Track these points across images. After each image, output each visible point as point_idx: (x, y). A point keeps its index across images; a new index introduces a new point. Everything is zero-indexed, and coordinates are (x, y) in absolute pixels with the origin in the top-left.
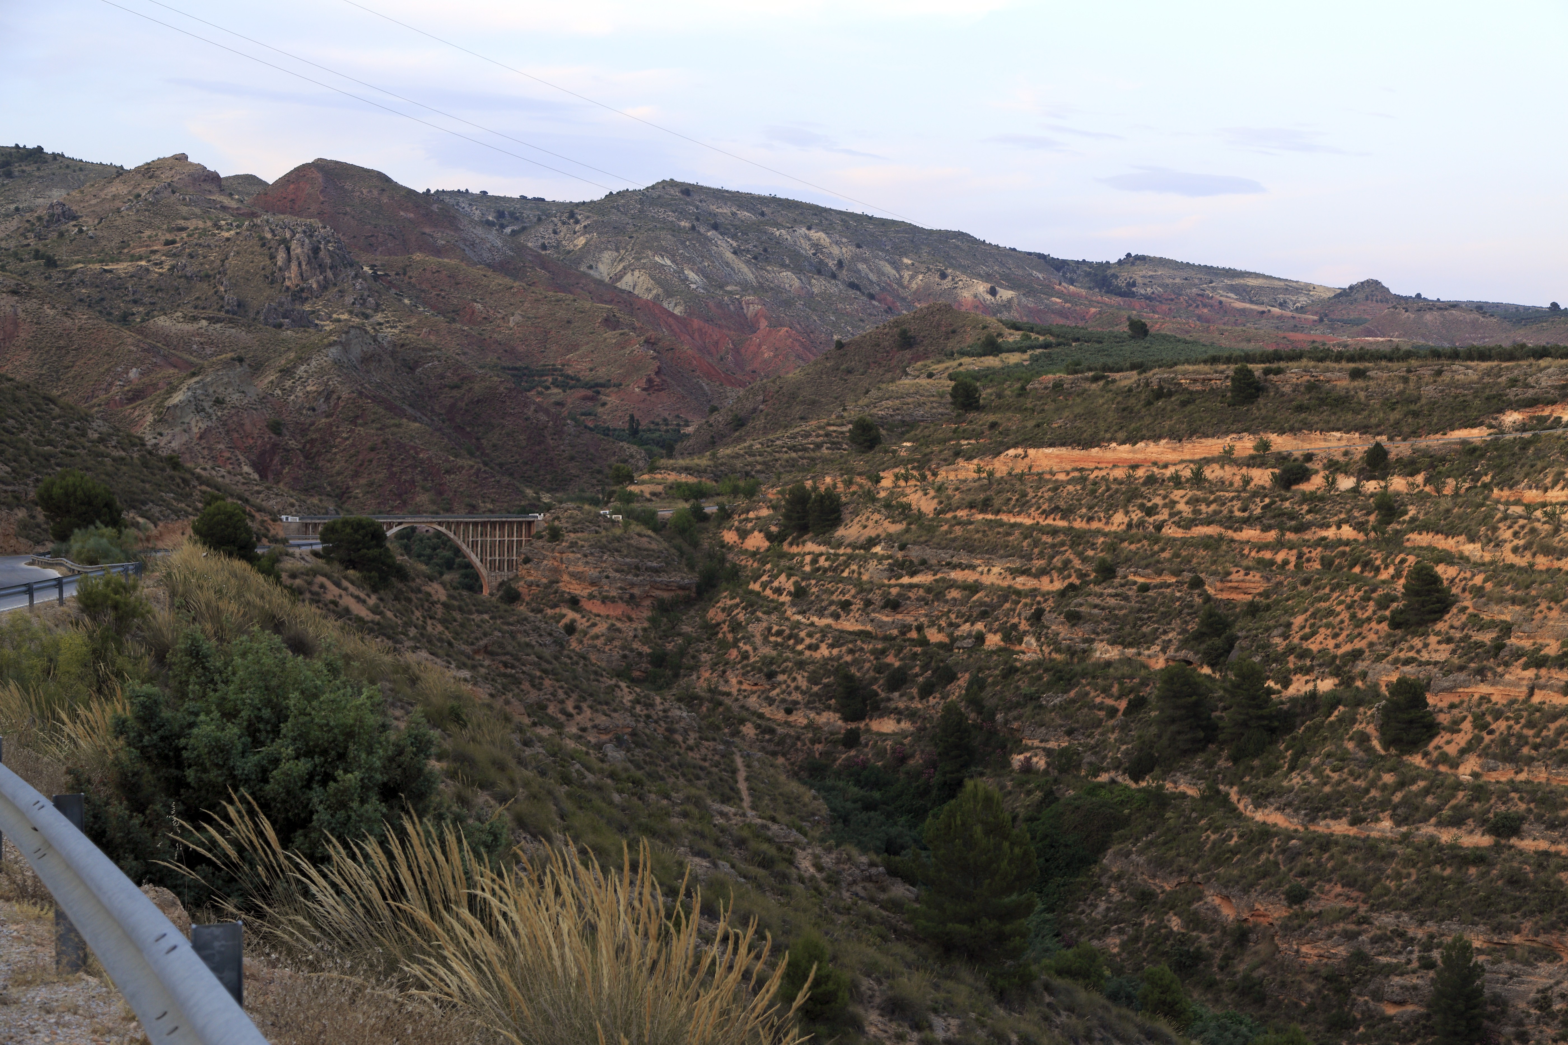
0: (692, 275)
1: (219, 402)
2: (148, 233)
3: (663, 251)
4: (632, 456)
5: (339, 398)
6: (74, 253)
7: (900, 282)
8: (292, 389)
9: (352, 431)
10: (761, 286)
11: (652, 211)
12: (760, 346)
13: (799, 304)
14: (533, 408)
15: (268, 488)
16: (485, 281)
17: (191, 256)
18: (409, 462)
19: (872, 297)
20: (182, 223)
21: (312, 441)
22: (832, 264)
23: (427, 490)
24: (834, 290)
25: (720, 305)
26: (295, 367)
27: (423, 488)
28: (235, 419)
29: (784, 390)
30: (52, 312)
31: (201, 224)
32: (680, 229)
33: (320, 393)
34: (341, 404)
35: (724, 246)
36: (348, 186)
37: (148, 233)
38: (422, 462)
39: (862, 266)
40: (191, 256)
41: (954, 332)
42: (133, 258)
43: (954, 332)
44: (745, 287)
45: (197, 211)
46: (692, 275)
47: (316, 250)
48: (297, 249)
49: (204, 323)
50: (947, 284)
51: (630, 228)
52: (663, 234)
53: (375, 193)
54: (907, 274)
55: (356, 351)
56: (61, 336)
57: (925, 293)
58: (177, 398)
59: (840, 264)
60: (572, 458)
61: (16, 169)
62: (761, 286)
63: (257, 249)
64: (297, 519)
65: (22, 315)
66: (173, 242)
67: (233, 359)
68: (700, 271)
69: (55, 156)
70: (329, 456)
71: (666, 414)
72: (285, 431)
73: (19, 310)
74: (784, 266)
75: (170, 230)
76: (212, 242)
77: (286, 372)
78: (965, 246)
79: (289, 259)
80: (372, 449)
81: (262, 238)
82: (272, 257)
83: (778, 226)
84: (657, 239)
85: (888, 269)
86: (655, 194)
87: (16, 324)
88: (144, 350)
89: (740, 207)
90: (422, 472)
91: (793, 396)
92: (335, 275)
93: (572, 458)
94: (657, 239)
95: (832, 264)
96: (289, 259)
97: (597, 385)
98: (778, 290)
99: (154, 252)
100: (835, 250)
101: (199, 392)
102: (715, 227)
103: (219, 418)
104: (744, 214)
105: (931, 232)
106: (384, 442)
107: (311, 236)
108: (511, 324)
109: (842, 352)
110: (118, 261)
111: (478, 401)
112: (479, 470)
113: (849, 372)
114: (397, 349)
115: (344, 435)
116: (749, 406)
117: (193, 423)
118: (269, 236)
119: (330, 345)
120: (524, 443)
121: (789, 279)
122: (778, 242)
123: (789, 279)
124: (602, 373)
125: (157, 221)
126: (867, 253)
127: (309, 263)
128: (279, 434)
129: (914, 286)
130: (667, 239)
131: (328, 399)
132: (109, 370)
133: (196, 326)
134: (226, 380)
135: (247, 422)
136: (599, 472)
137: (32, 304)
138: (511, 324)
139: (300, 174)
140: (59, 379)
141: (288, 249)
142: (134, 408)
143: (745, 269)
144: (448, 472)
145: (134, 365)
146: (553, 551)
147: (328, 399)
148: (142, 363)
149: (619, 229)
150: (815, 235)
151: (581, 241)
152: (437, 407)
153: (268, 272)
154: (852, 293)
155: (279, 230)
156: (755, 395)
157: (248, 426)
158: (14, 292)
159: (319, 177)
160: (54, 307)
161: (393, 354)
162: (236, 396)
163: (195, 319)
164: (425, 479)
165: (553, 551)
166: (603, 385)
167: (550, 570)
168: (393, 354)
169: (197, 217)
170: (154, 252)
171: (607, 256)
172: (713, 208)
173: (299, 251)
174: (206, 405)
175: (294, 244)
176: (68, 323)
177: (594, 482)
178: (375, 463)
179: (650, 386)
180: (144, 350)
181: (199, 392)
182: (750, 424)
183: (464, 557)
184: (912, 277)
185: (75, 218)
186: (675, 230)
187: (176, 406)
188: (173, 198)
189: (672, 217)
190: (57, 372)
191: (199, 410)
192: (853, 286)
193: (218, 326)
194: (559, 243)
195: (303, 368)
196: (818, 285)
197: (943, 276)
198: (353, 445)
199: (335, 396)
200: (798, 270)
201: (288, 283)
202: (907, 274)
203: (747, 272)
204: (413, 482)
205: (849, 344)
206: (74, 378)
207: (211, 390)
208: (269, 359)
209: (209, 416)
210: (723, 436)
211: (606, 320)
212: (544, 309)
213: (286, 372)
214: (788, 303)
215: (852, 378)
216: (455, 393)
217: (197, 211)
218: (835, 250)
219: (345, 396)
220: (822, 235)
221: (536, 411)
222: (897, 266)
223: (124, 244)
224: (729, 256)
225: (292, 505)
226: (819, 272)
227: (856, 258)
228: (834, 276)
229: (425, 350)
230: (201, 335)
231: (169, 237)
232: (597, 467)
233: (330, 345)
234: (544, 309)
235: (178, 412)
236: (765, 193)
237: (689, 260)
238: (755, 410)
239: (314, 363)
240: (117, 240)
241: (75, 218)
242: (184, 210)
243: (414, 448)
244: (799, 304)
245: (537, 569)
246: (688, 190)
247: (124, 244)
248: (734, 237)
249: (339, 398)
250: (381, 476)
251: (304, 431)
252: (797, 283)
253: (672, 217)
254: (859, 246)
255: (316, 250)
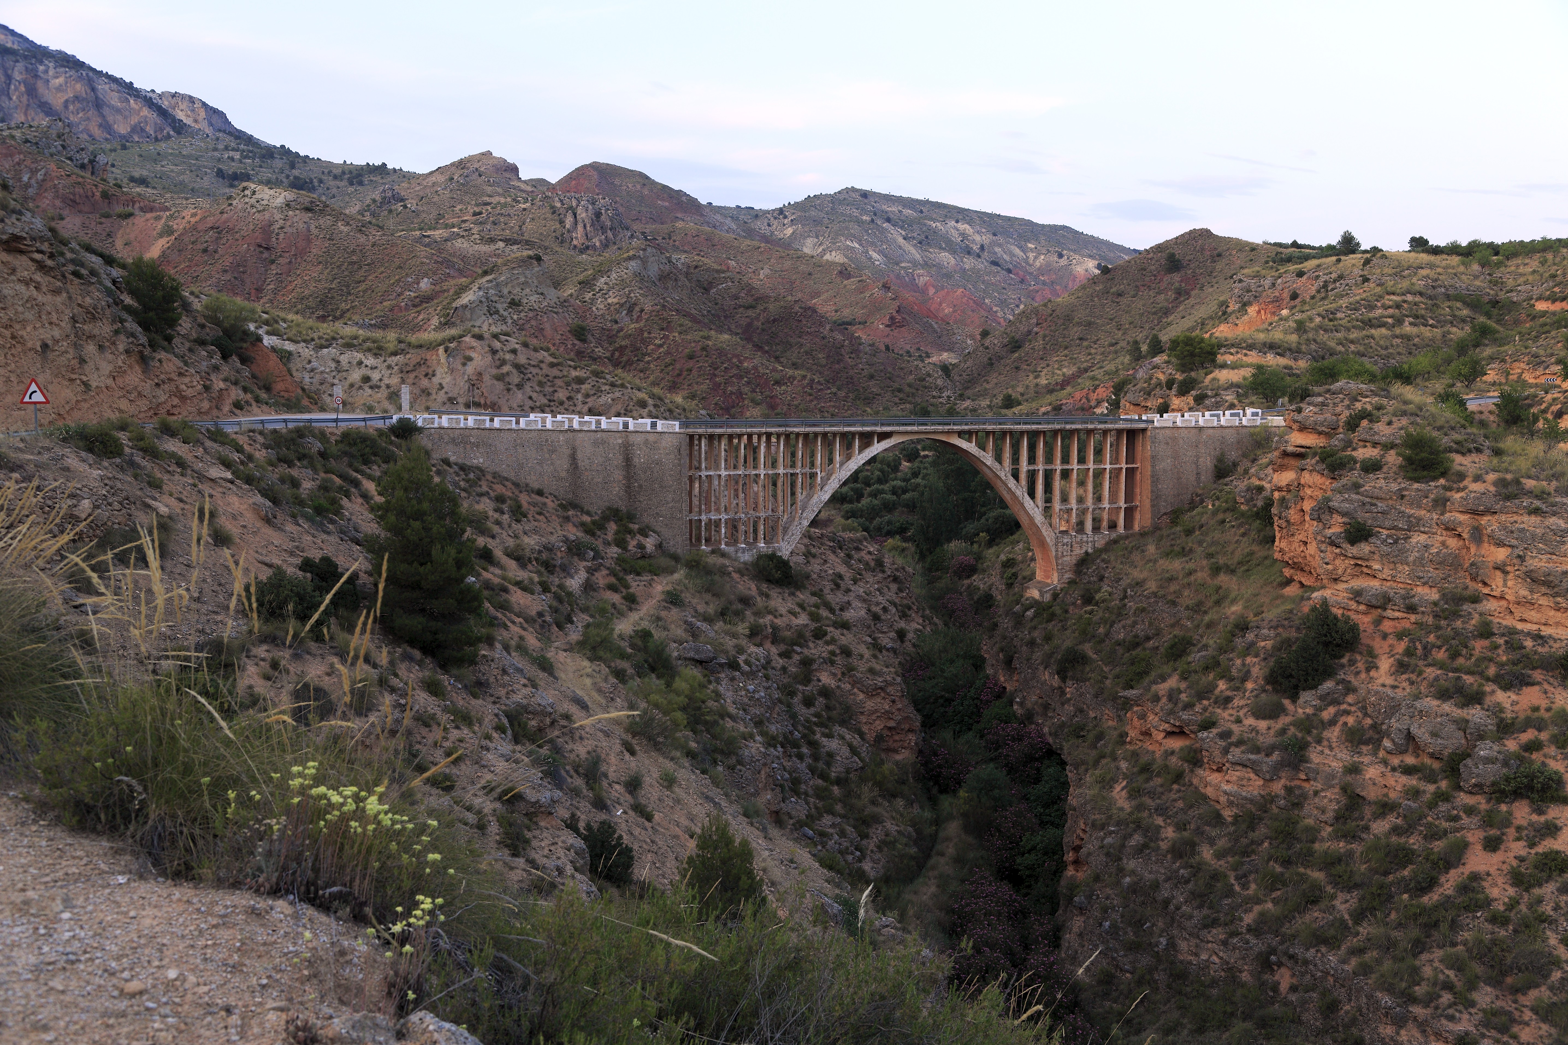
0: (875, 255)
1: (514, 304)
2: (459, 207)
3: (852, 237)
4: (929, 375)
5: (642, 311)
6: (399, 224)
7: (1026, 260)
8: (593, 301)
9: (665, 337)
10: (926, 263)
11: (841, 209)
12: (940, 304)
13: (957, 277)
14: (828, 327)
15: (597, 374)
16: (736, 243)
17: (494, 223)
18: (735, 371)
19: (1009, 271)
20: (487, 199)
21: (622, 349)
22: (976, 248)
23: (757, 404)
24: (981, 266)
25: (898, 276)
26: (594, 279)
27: (753, 401)
28: (533, 323)
29: (1058, 312)
30: (345, 229)
31: (502, 200)
32: (863, 222)
33: (622, 305)
34: (645, 316)
35: (896, 235)
36: (617, 182)
37: (459, 207)
38: (747, 372)
39: (998, 250)
40: (494, 223)
41: (1219, 255)
42: (446, 226)
43: (1219, 255)
44: (915, 264)
45: (500, 190)
46: (875, 255)
47: (598, 215)
48: (582, 214)
49: (501, 244)
50: (1063, 262)
51: (826, 221)
52: (851, 225)
53: (638, 187)
54: (1031, 255)
55: (654, 270)
56: (354, 251)
57: (1046, 269)
58: (467, 298)
59: (982, 248)
60: (872, 377)
61: (366, 180)
62: (926, 263)
63: (549, 215)
64: (675, 425)
65: (315, 231)
66: (480, 213)
67: (530, 257)
68: (880, 252)
69: (394, 170)
70: (641, 365)
71: (908, 347)
72: (590, 337)
73: (312, 227)
74: (941, 248)
75: (477, 205)
76: (512, 212)
77: (586, 284)
78: (1070, 236)
79: (576, 223)
80: (691, 357)
81: (553, 207)
82: (562, 222)
83: (935, 220)
84: (847, 228)
85: (1017, 251)
86: (842, 197)
87: (309, 240)
88: (436, 262)
89: (905, 206)
90: (748, 383)
91: (1068, 318)
92: (615, 236)
93: (872, 377)
94: (847, 228)
95: (976, 248)
96: (576, 223)
97: (844, 323)
98: (939, 266)
99: (464, 221)
100: (977, 238)
101: (492, 292)
102: (888, 220)
103: (514, 322)
104: (908, 212)
105: (1043, 226)
106: (704, 349)
107: (593, 204)
108: (762, 277)
109: (1108, 276)
110: (435, 229)
111: (774, 321)
112: (812, 380)
113: (1120, 295)
114: (690, 271)
115: (658, 342)
116: (1023, 328)
117: (485, 327)
118: (558, 205)
119: (630, 258)
120: (824, 361)
121: (946, 258)
122: (935, 232)
123: (946, 258)
124: (846, 313)
125: (467, 198)
126: (1000, 239)
127: (592, 225)
128: (584, 341)
129: (1038, 264)
130: (855, 229)
131: (630, 311)
132: (399, 280)
133: (493, 247)
134: (522, 279)
135: (547, 326)
136: (900, 390)
137: (326, 221)
138: (762, 277)
139: (580, 173)
140: (349, 294)
141: (575, 215)
142: (419, 312)
143: (913, 251)
144: (777, 383)
145: (426, 275)
146: (1441, 504)
147: (630, 311)
148: (435, 273)
149: (817, 222)
150: (960, 226)
151: (789, 231)
152: (733, 327)
153: (558, 234)
154: (994, 268)
155: (566, 200)
156: (1028, 318)
157: (548, 331)
158: (308, 209)
159: (595, 175)
160: (348, 224)
161: (687, 274)
162: (534, 298)
163: (492, 240)
164: (754, 391)
165: (1441, 504)
166: (850, 324)
167: (1440, 562)
168: (687, 274)
169: (499, 195)
170: (464, 221)
171: (810, 242)
172: (884, 207)
173: (584, 215)
174: (500, 307)
175: (579, 210)
176: (362, 239)
177: (897, 400)
178: (695, 372)
179: (892, 323)
180: (436, 262)
181: (492, 292)
182: (1027, 347)
183: (1003, 505)
184: (1036, 258)
185: (402, 200)
186: (860, 222)
187: (465, 307)
188: (480, 180)
189: (856, 213)
190: (348, 286)
191: (492, 312)
192: (995, 263)
193: (515, 247)
194: (772, 233)
195: (603, 280)
196: (969, 263)
197: (1061, 256)
198: (668, 353)
199: (637, 309)
200: (953, 252)
201: (575, 242)
202: (1031, 255)
203: (915, 253)
204: (740, 395)
205: (1115, 269)
206: (365, 291)
207: (505, 291)
208: (566, 279)
209: (504, 320)
210: (1000, 358)
211: (841, 272)
212: (788, 264)
213: (586, 284)
214: (948, 276)
215: (1124, 301)
216: (750, 313)
217: (500, 190)
218: (977, 238)
219: (648, 308)
220: (967, 226)
221: (831, 330)
222: (1024, 250)
223: (440, 216)
224: (901, 240)
225: (643, 404)
226: (969, 253)
227: (993, 244)
228: (979, 256)
229: (718, 271)
230: (498, 256)
231: (477, 210)
232: (896, 385)
233: (630, 258)
234: (788, 264)
235: (468, 314)
236: (921, 197)
237: (873, 244)
238: (1029, 332)
239: (614, 275)
240: (434, 213)
241: (402, 200)
242: (489, 190)
243: (737, 356)
244: (957, 277)
245: (1395, 558)
246: (865, 194)
247: (440, 216)
248: (902, 228)
249: (642, 311)
250: (704, 387)
251: (611, 338)
252: (953, 261)
253: (856, 213)
254: (995, 235)
255: (598, 215)
